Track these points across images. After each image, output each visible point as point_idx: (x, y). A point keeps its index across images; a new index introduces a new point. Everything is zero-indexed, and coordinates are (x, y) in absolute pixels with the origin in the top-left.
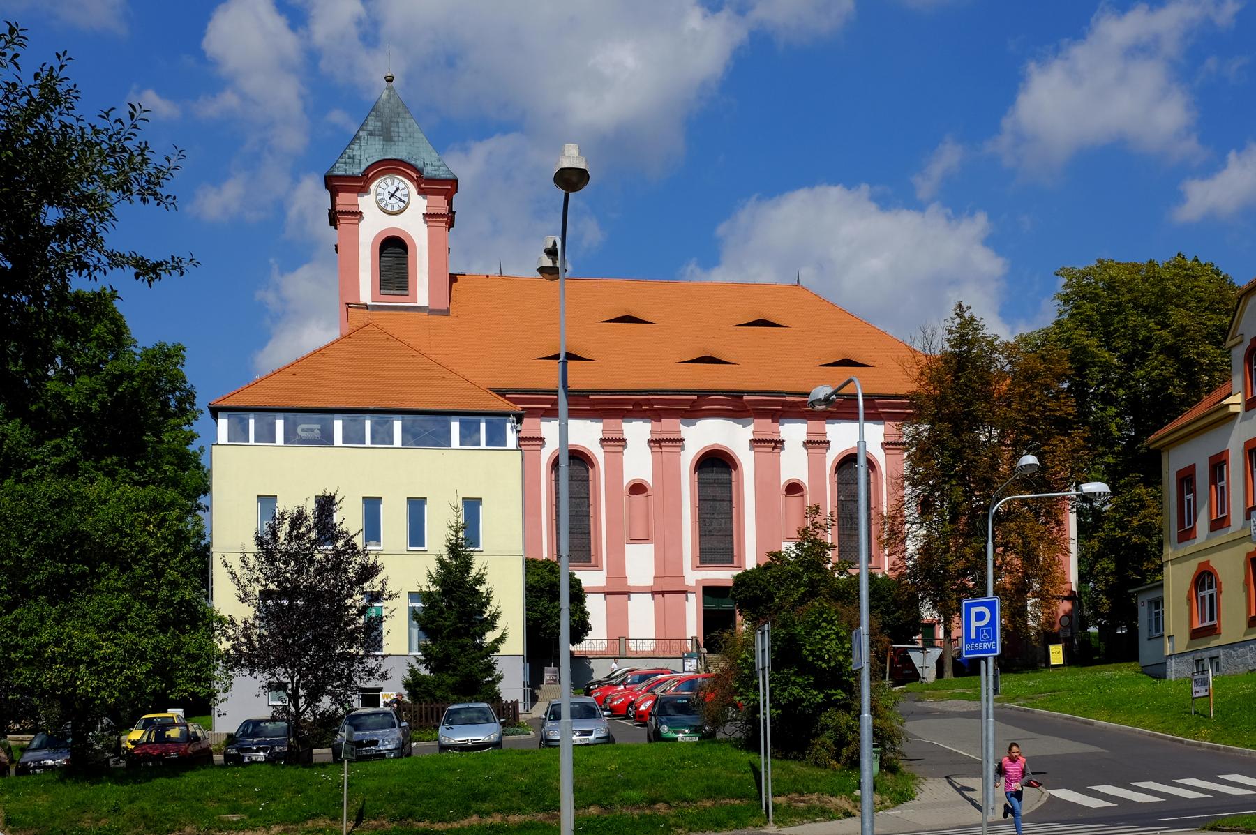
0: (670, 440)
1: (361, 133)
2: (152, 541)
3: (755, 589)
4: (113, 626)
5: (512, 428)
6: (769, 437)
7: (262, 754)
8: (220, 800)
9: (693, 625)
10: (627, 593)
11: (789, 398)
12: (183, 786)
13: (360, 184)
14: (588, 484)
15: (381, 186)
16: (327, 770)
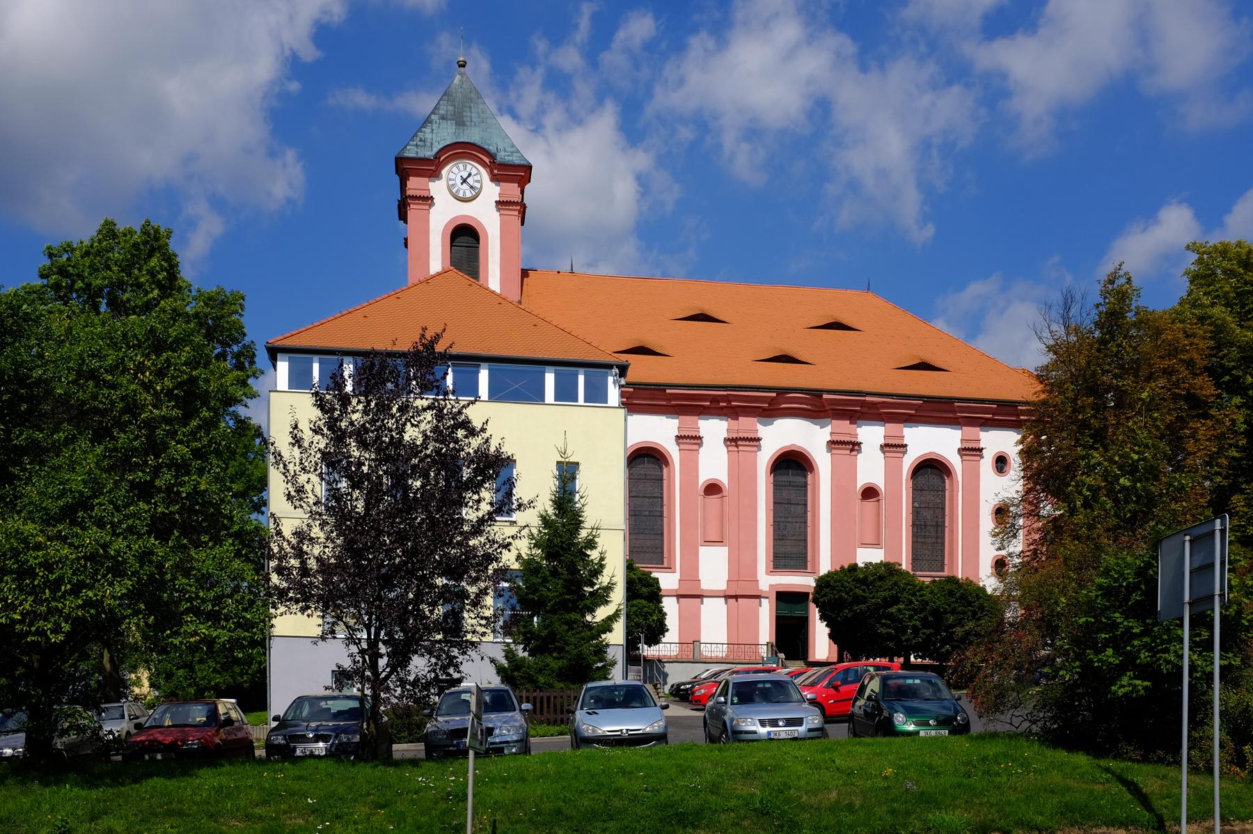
0: (747, 439)
1: (433, 117)
2: (148, 398)
3: (841, 591)
4: (68, 514)
5: (614, 382)
6: (847, 439)
7: (321, 744)
8: (248, 817)
9: (765, 632)
10: (700, 597)
11: (868, 399)
12: (189, 792)
13: (431, 168)
14: (662, 483)
15: (454, 171)
16: (424, 770)
